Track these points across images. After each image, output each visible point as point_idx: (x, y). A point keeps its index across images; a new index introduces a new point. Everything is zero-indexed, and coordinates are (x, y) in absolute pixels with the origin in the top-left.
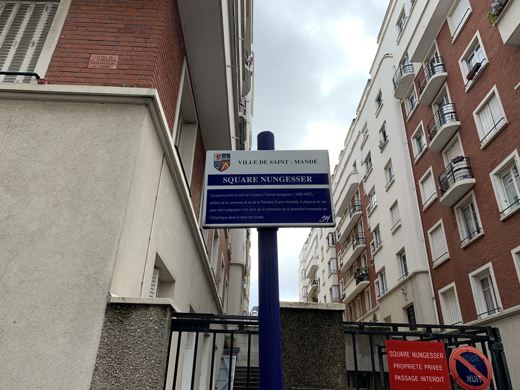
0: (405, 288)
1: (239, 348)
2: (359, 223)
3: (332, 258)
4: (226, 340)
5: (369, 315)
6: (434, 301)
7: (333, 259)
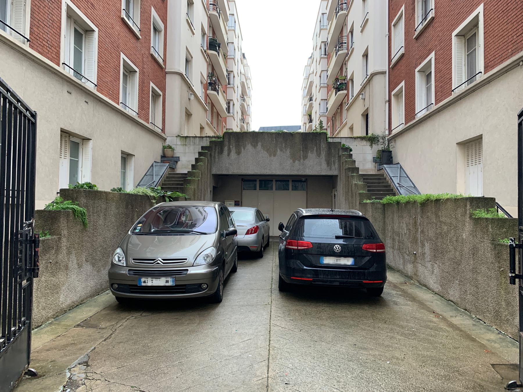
0: (365, 93)
1: (179, 157)
3: (323, 71)
4: (164, 150)
6: (387, 104)
7: (324, 71)
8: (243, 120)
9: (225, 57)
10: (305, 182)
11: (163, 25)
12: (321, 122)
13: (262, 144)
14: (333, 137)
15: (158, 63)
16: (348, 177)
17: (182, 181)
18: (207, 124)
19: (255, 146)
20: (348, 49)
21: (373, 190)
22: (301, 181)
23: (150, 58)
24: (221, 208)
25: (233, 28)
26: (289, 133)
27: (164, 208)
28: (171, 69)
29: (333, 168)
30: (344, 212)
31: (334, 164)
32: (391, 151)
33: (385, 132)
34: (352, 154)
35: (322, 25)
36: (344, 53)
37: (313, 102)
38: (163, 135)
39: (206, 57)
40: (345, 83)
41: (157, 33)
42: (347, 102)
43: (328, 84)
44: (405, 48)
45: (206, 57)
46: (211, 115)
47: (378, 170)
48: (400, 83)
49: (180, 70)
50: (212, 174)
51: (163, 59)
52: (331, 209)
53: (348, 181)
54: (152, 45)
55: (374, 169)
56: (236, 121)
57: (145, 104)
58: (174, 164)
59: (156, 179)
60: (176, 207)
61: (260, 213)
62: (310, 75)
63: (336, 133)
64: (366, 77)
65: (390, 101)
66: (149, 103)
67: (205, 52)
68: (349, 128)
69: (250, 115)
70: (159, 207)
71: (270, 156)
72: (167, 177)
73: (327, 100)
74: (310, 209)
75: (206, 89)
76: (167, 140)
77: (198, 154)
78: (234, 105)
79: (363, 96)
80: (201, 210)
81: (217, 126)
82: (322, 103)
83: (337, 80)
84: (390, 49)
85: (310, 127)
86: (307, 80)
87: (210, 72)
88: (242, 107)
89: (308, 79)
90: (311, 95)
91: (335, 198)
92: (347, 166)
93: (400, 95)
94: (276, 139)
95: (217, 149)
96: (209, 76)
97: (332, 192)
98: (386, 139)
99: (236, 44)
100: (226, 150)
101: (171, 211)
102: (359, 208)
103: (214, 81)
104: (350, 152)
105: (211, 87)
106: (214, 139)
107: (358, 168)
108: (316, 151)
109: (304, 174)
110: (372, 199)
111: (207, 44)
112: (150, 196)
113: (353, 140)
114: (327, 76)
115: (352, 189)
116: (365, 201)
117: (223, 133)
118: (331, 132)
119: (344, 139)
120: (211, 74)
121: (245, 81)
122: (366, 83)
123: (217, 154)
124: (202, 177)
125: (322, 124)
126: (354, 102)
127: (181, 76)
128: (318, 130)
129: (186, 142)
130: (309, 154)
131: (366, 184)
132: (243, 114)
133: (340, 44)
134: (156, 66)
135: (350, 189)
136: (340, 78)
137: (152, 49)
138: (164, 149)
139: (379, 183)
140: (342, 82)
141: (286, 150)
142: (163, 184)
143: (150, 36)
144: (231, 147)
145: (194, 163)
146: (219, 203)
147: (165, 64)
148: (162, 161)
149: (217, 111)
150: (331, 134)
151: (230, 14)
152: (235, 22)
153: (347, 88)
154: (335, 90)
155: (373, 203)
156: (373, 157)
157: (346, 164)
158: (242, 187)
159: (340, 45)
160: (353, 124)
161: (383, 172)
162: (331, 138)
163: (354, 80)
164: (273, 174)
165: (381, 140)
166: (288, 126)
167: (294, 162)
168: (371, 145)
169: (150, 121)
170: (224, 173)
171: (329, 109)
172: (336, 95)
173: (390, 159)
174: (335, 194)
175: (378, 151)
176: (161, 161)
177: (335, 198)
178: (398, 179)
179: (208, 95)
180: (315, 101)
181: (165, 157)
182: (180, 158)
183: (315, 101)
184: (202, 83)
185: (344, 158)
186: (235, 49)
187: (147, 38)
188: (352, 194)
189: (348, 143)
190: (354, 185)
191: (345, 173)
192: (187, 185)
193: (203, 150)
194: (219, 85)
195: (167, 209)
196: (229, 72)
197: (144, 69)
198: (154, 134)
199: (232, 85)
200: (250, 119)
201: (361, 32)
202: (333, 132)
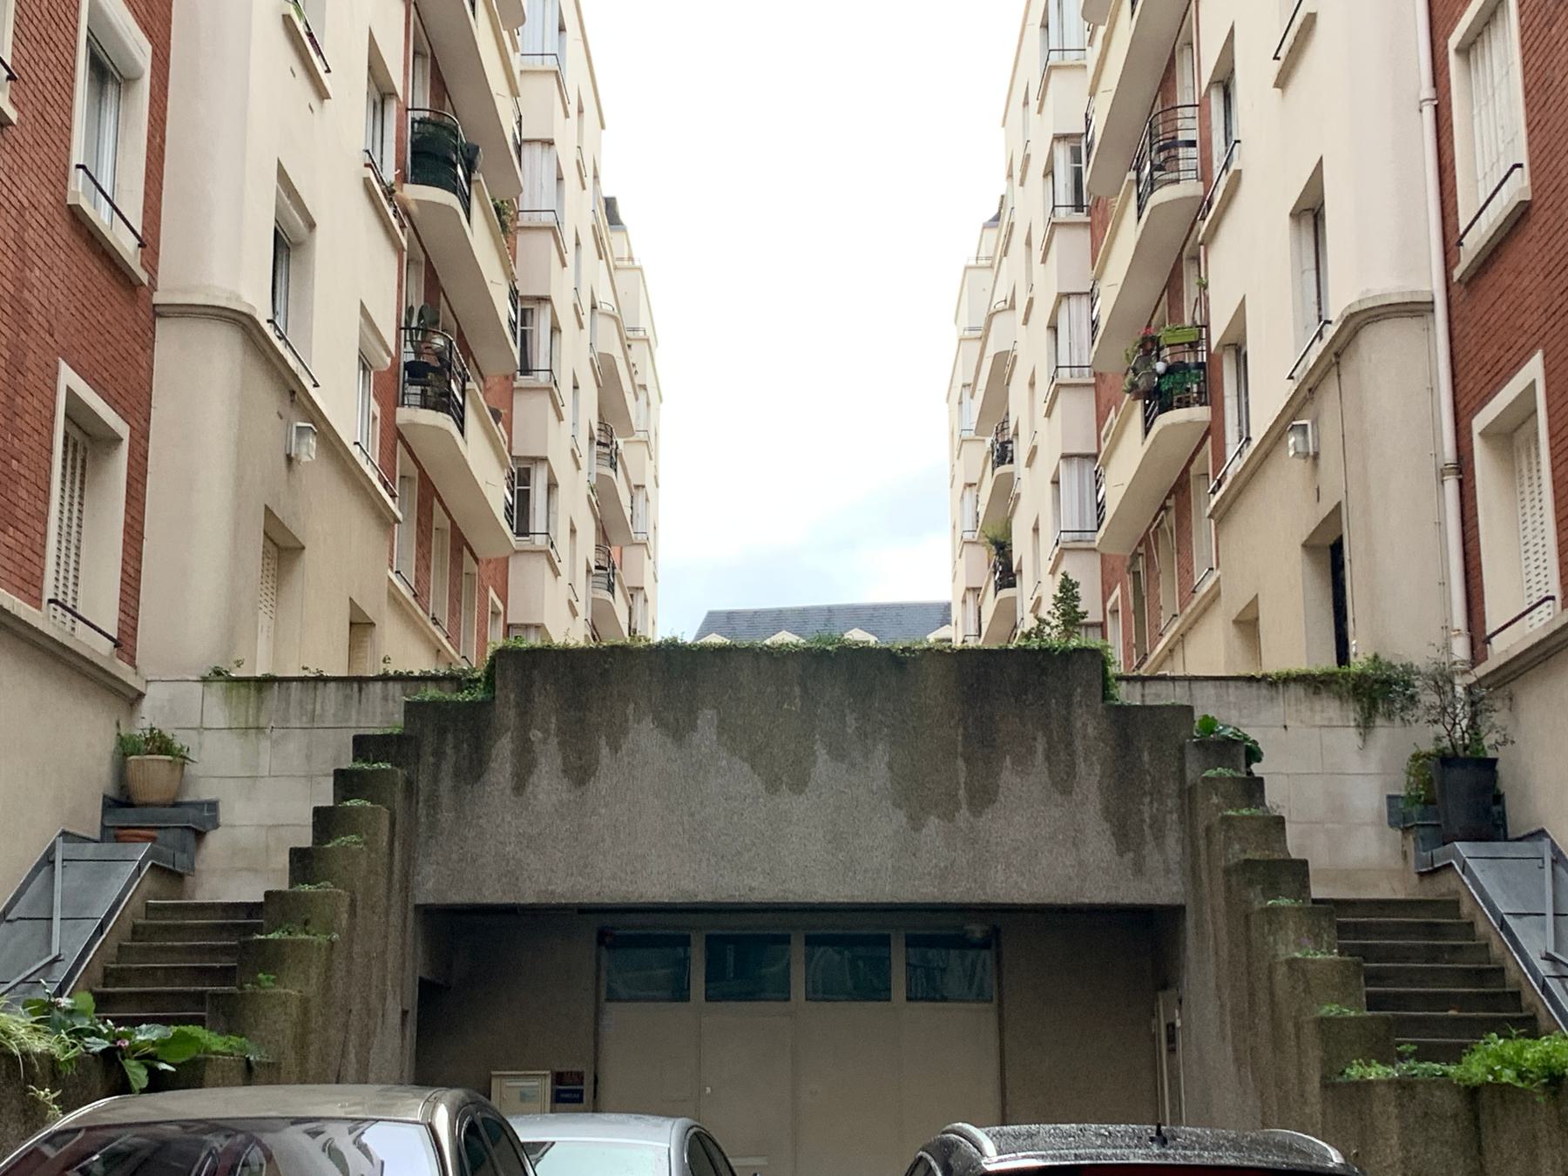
0: (1315, 422)
1: (213, 806)
2: (1182, 50)
3: (1068, 295)
5: (1205, 610)
6: (1451, 485)
7: (1073, 300)
8: (605, 572)
9: (505, 220)
10: (985, 945)
11: (148, 48)
12: (1068, 590)
13: (722, 721)
14: (1141, 672)
15: (111, 260)
16: (1247, 917)
17: (226, 950)
18: (394, 598)
19: (679, 731)
20: (1205, 176)
21: (1399, 1001)
22: (961, 942)
23: (63, 230)
24: (472, 1129)
25: (550, 63)
26: (880, 651)
27: (112, 1133)
28: (186, 291)
29: (1153, 859)
30: (1236, 1146)
31: (1159, 837)
32: (1494, 761)
33: (1447, 647)
34: (1261, 779)
35: (1054, 44)
36: (1186, 198)
37: (1019, 466)
38: (122, 670)
39: (394, 221)
40: (1200, 366)
41: (111, 90)
42: (1215, 473)
43: (1099, 370)
44: (1532, 173)
45: (394, 221)
46: (420, 544)
47: (1421, 874)
48: (1518, 366)
49: (238, 298)
50: (417, 907)
51: (139, 231)
52: (1151, 1130)
53: (1248, 942)
54: (77, 157)
55: (1400, 865)
56: (564, 579)
57: (24, 494)
58: (184, 851)
59: (68, 941)
60: (185, 1124)
61: (713, 1150)
62: (991, 316)
63: (1160, 647)
64: (1320, 334)
65: (1463, 468)
66: (49, 483)
67: (389, 192)
68: (1235, 622)
69: (651, 544)
70: (78, 1130)
71: (772, 786)
72: (136, 932)
73: (1096, 457)
74: (1024, 1128)
75: (390, 399)
76: (146, 704)
77: (331, 779)
78: (552, 486)
79: (1306, 442)
80: (344, 1143)
81: (454, 612)
82: (1071, 477)
83: (1150, 346)
84: (1448, 181)
85: (1007, 611)
86: (978, 344)
87: (418, 303)
88: (604, 501)
89: (984, 339)
90: (1002, 429)
91: (1172, 1050)
92: (1237, 853)
93: (1520, 437)
94: (805, 690)
95: (449, 751)
96: (408, 327)
97: (1153, 1014)
98: (1459, 690)
99: (566, 151)
100: (508, 753)
101: (157, 1150)
102: (1324, 1114)
103: (439, 355)
104: (1248, 765)
105: (417, 389)
106: (431, 692)
107: (1305, 863)
108: (1048, 758)
109: (979, 897)
110: (1402, 1057)
111: (400, 151)
112: (26, 1054)
113: (1264, 692)
114: (1094, 324)
115: (1272, 994)
116: (1354, 1072)
117: (489, 654)
118: (1127, 644)
119: (1210, 689)
120: (421, 316)
121: (617, 352)
122: (1322, 365)
123: (446, 783)
124: (352, 927)
125: (1077, 598)
126: (1253, 474)
127: (244, 327)
128: (1053, 636)
129: (259, 709)
130: (1008, 777)
131: (1358, 965)
132: (605, 537)
133: (1160, 150)
134: (95, 267)
135: (1262, 996)
136: (1164, 336)
137: (78, 181)
138: (125, 755)
139: (1434, 954)
140: (1179, 357)
141: (866, 755)
142: (109, 976)
143: (68, 111)
144: (536, 735)
145: (306, 840)
146: (458, 1093)
147: (151, 263)
148: (112, 833)
149: (453, 523)
150: (1128, 657)
151: (522, 72)
152: (562, 29)
153: (1209, 395)
154: (1139, 403)
155: (1404, 1085)
156: (1390, 797)
157: (1228, 842)
158: (598, 978)
159: (1162, 156)
160: (1257, 596)
161: (1454, 884)
162: (1129, 679)
163: (1251, 348)
164: (791, 898)
165: (1429, 698)
166: (875, 608)
167: (916, 824)
168: (1366, 726)
169: (48, 594)
170: (493, 895)
171: (1110, 511)
172: (1147, 431)
173: (1488, 811)
174: (1171, 1027)
175: (1416, 757)
176: (104, 828)
177: (1172, 1050)
178: (1543, 928)
179: (401, 436)
180: (1029, 464)
181: (131, 805)
182: (222, 808)
183: (1029, 464)
184: (365, 366)
185: (1215, 800)
186: (560, 179)
187: (52, 116)
188: (1276, 1023)
189: (1234, 712)
190: (1282, 972)
191: (1229, 889)
192: (258, 983)
193: (366, 760)
194: (466, 379)
195: (126, 1140)
196: (527, 306)
197: (26, 293)
198: (69, 665)
199: (543, 378)
200: (648, 564)
201: (1276, 85)
202: (1138, 646)
